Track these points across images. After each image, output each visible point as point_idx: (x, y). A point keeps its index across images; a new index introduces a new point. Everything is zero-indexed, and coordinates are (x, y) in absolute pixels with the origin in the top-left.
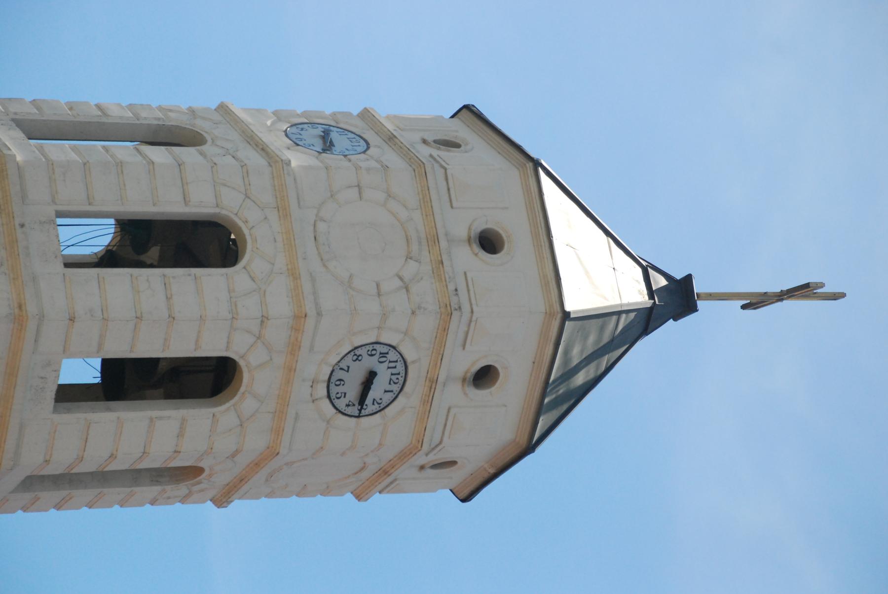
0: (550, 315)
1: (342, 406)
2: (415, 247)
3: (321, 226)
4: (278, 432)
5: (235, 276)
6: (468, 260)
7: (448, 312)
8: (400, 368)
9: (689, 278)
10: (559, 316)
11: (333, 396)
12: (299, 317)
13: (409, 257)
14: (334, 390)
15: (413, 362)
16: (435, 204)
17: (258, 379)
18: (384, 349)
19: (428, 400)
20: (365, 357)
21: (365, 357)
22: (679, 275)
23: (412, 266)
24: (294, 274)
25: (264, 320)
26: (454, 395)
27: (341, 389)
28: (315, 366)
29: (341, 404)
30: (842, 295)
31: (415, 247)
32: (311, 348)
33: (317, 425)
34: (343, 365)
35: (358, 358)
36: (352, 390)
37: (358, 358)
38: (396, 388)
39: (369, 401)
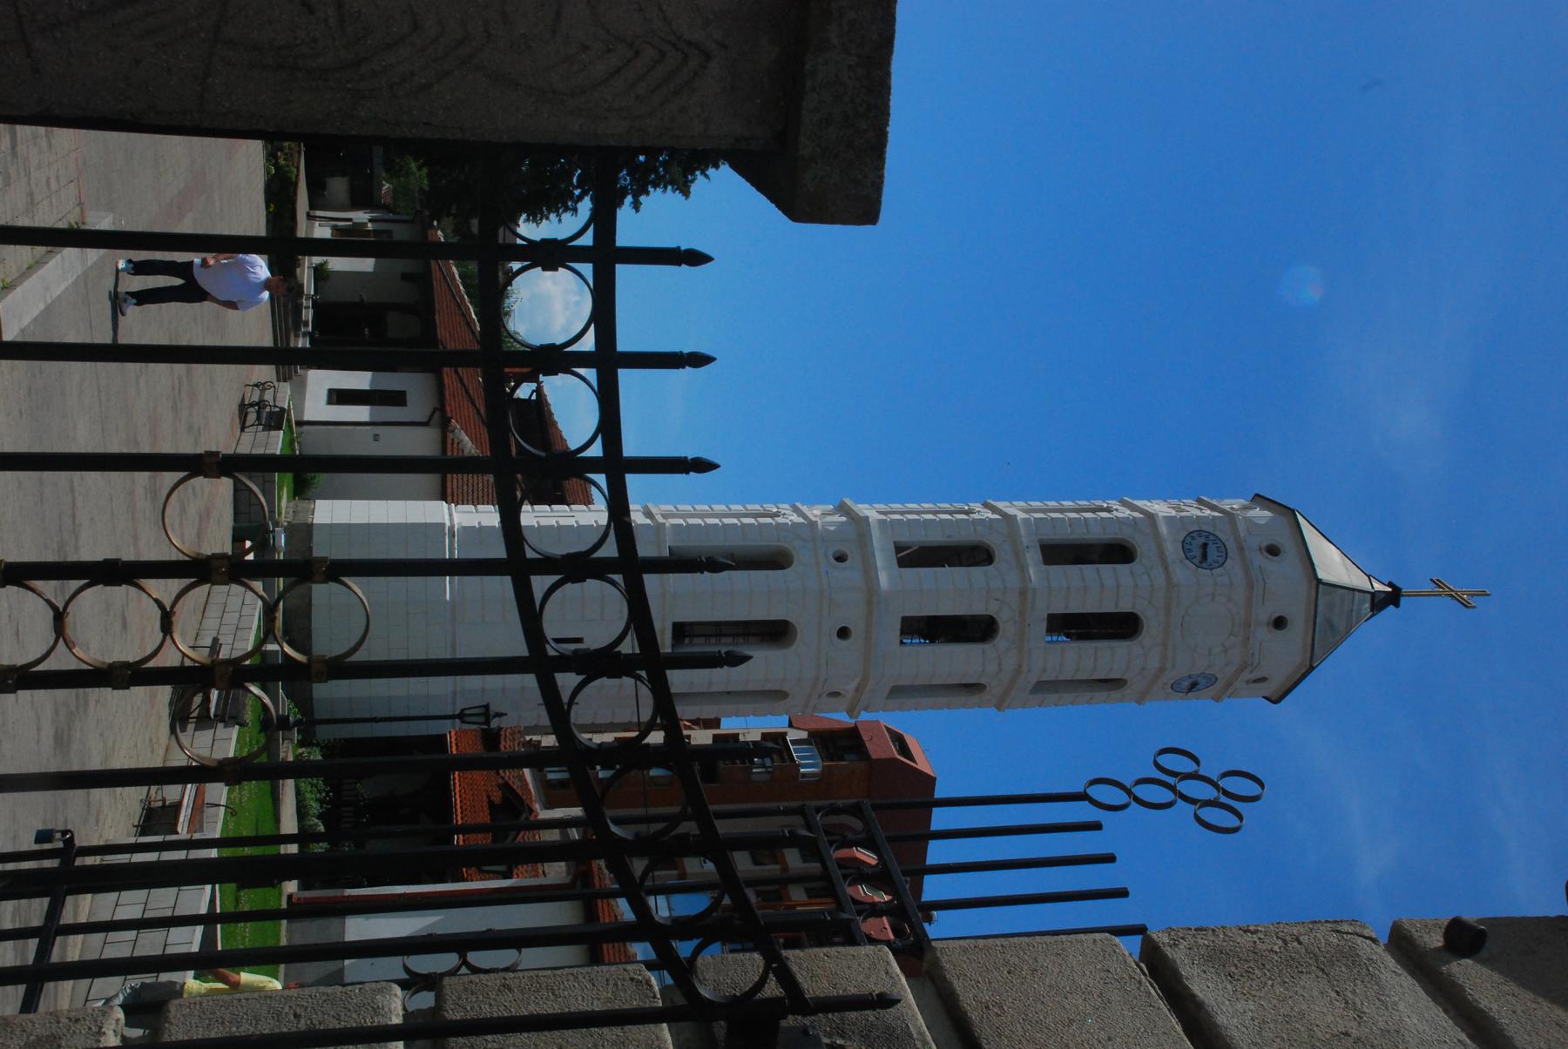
26: (1260, 560)
36: (1197, 552)
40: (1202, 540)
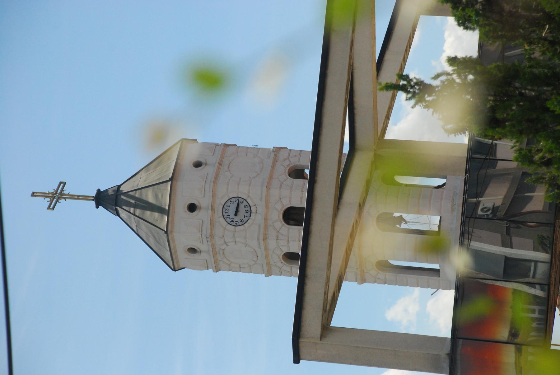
0: (172, 232)
1: (245, 202)
2: (221, 252)
3: (255, 259)
4: (268, 195)
5: (286, 250)
6: (202, 246)
7: (211, 236)
8: (225, 215)
9: (97, 207)
10: (169, 232)
11: (249, 207)
12: (265, 239)
13: (223, 250)
14: (248, 209)
15: (220, 217)
16: (213, 263)
17: (277, 216)
18: (232, 223)
19: (213, 202)
20: (239, 221)
21: (239, 221)
22: (94, 194)
23: (223, 247)
24: (266, 250)
25: (277, 239)
26: (203, 201)
27: (246, 209)
28: (257, 218)
29: (245, 203)
30: (33, 194)
31: (221, 252)
32: (260, 226)
33: (253, 194)
34: (247, 219)
35: (242, 221)
36: (242, 208)
37: (242, 221)
38: (225, 207)
39: (236, 204)
40: (237, 219)
